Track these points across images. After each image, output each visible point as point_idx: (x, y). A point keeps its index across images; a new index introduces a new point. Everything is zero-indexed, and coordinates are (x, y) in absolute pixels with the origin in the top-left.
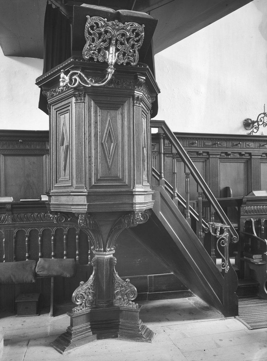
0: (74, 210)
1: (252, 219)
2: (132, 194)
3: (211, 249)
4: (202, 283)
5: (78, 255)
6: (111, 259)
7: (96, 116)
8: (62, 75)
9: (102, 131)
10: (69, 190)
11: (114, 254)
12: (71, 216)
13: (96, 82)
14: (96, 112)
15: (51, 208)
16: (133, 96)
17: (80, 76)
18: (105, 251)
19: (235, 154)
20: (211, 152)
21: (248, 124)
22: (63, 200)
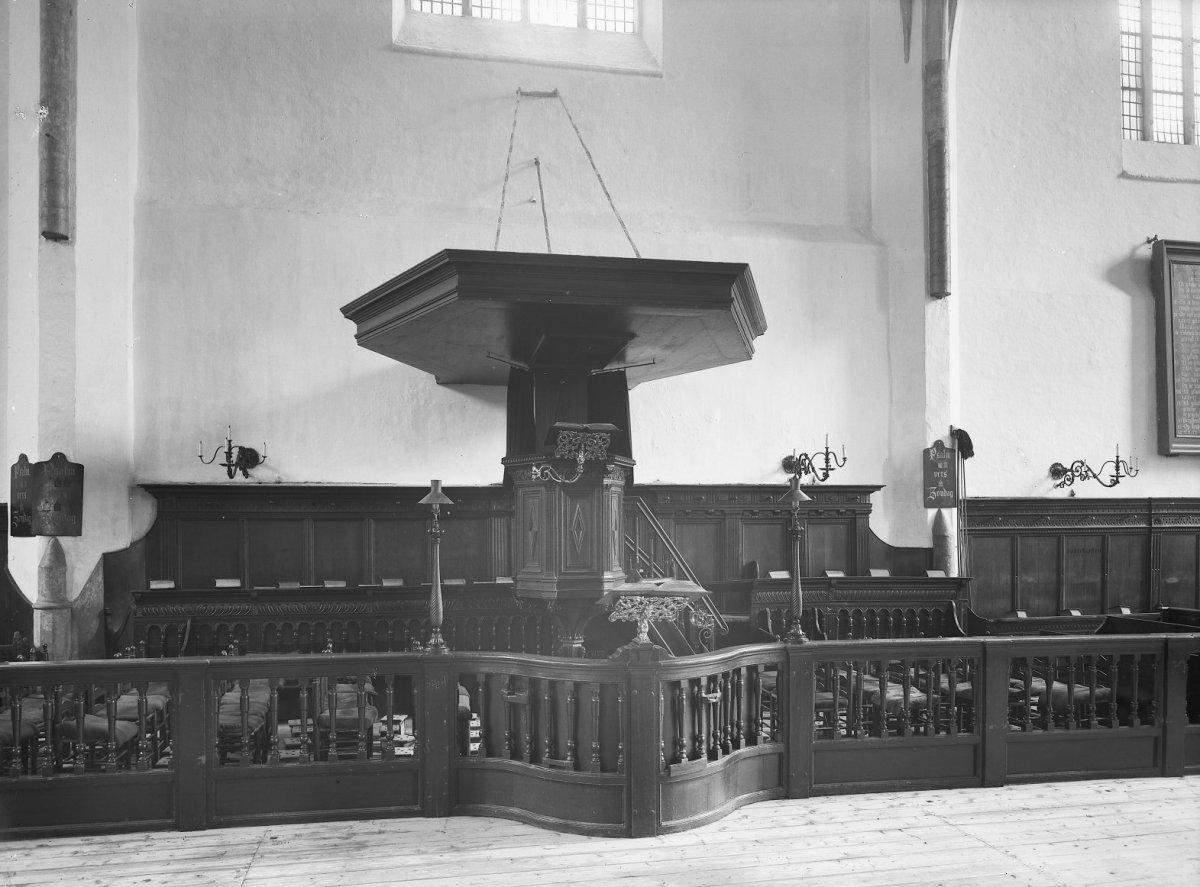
0: (545, 596)
1: (768, 609)
2: (601, 582)
3: (394, 693)
4: (208, 661)
5: (466, 717)
6: (580, 648)
7: (565, 506)
8: (534, 468)
9: (571, 521)
10: (540, 576)
11: (582, 644)
12: (542, 602)
13: (566, 479)
14: (565, 502)
15: (599, 28)
16: (602, 485)
17: (551, 471)
18: (573, 639)
19: (766, 513)
20: (727, 510)
21: (789, 464)
22: (532, 586)
